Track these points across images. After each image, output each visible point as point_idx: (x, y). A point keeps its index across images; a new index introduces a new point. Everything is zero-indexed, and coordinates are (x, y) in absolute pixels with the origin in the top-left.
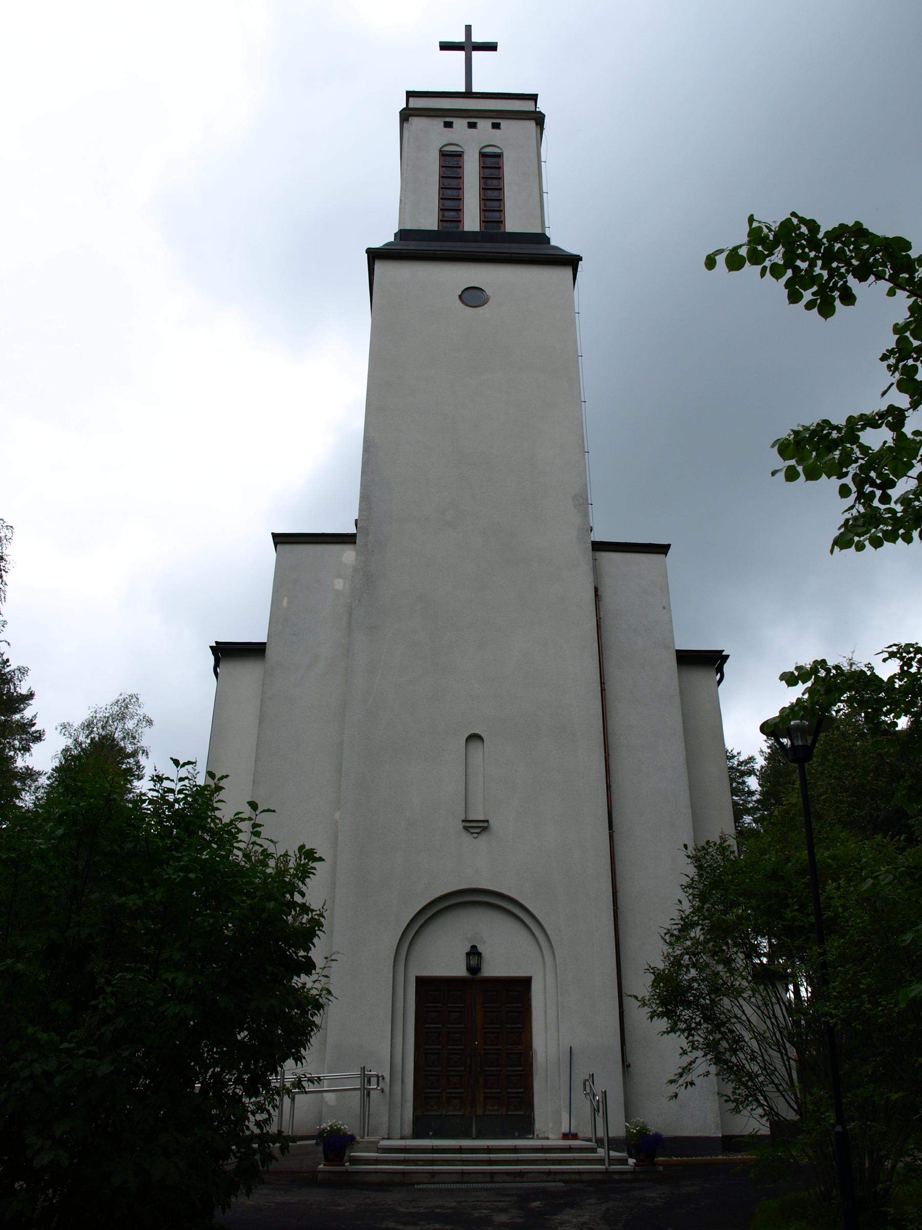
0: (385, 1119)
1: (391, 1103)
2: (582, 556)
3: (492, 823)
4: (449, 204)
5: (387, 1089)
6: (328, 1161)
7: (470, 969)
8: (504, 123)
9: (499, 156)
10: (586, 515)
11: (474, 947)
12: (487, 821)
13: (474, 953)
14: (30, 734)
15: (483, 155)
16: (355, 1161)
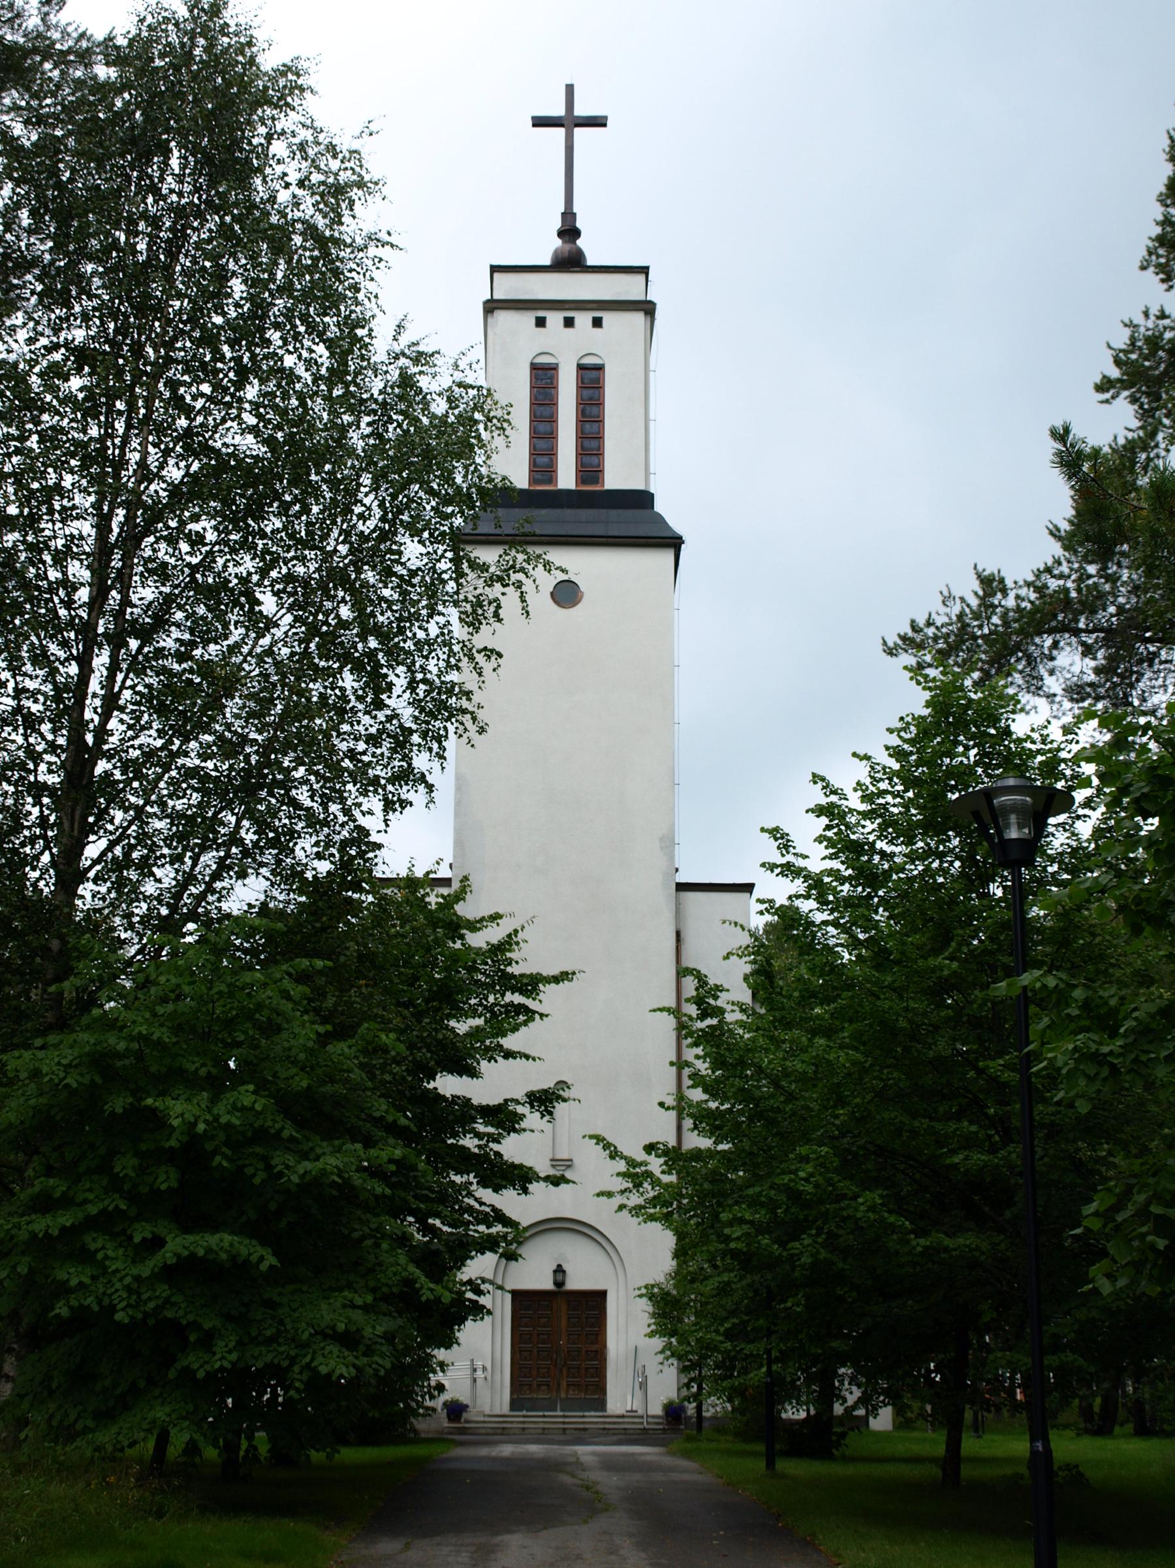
0: (489, 1400)
1: (492, 1388)
2: (663, 897)
3: (576, 1161)
4: (542, 427)
5: (489, 1378)
6: (450, 1420)
7: (556, 1283)
8: (608, 317)
9: (600, 368)
10: (671, 857)
11: (559, 1266)
12: (571, 1160)
13: (559, 1270)
14: (1094, 855)
15: (581, 368)
16: (467, 1422)
